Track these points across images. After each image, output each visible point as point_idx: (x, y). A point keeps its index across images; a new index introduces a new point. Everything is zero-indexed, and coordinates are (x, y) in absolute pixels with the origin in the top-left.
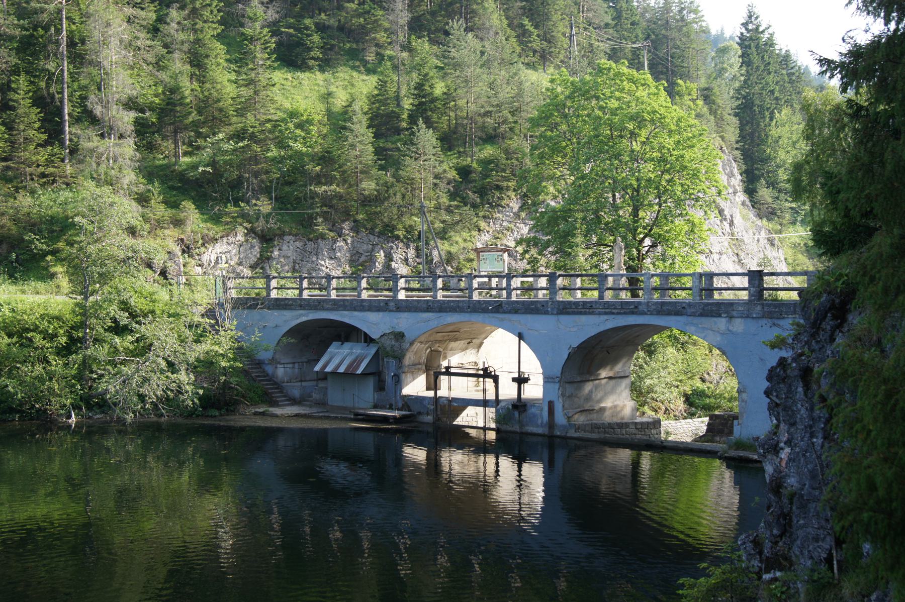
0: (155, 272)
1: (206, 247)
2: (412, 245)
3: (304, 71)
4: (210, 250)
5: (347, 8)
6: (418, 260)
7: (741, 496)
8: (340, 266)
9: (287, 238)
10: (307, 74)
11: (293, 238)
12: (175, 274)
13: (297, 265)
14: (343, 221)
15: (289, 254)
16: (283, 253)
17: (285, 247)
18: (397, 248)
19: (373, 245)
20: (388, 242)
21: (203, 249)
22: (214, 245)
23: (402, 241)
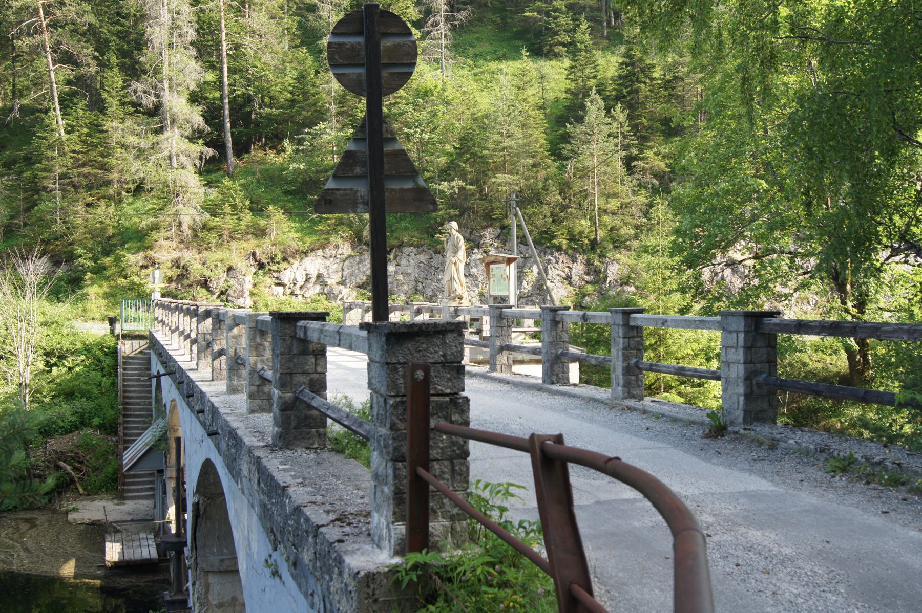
0: (212, 293)
1: (289, 262)
2: (580, 258)
3: (551, 60)
4: (295, 266)
5: (770, 324)
6: (587, 278)
7: (427, 526)
8: (477, 286)
9: (407, 250)
10: (553, 63)
11: (415, 250)
12: (235, 295)
13: (420, 284)
14: (484, 228)
15: (409, 271)
16: (401, 269)
17: (404, 262)
18: (557, 262)
19: (525, 258)
20: (545, 254)
21: (284, 265)
22: (302, 259)
23: (566, 253)
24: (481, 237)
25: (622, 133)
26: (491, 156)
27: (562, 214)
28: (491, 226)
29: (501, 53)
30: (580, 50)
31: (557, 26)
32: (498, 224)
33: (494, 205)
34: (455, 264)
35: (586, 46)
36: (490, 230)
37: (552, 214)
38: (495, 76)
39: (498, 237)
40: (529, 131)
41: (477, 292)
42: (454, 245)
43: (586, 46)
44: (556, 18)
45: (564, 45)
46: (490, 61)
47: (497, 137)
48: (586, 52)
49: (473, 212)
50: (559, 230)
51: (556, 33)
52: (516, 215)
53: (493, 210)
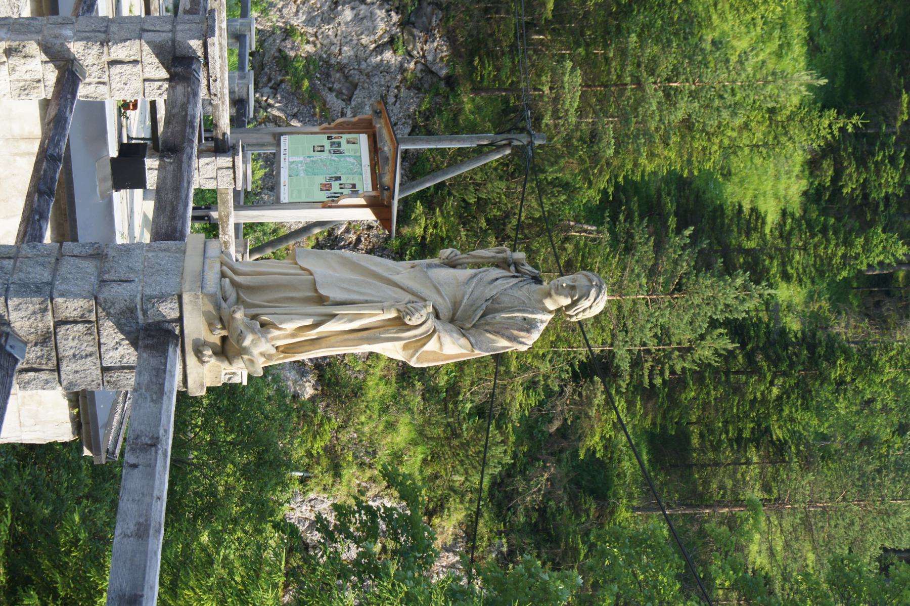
8: (310, 21)
14: (450, 37)
24: (428, 31)
25: (668, 356)
26: (623, 53)
27: (483, 224)
28: (455, 52)
29: (822, 40)
30: (848, 243)
31: (876, 164)
32: (459, 70)
33: (507, 61)
34: (399, 323)
35: (857, 257)
36: (445, 52)
37: (482, 204)
38: (776, 33)
39: (427, 70)
40: (674, 139)
41: (294, 22)
42: (492, 307)
43: (857, 257)
44: (893, 160)
45: (836, 178)
46: (808, 19)
47: (664, 69)
48: (844, 256)
49: (487, 10)
50: (446, 217)
51: (862, 162)
52: (495, 147)
53: (491, 54)
